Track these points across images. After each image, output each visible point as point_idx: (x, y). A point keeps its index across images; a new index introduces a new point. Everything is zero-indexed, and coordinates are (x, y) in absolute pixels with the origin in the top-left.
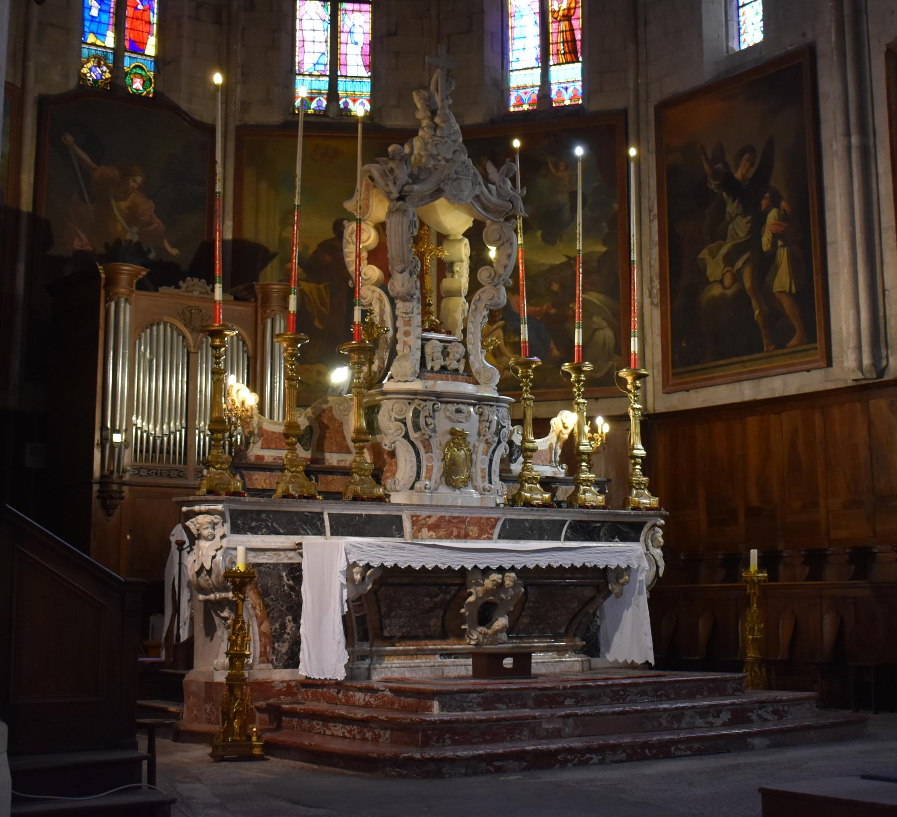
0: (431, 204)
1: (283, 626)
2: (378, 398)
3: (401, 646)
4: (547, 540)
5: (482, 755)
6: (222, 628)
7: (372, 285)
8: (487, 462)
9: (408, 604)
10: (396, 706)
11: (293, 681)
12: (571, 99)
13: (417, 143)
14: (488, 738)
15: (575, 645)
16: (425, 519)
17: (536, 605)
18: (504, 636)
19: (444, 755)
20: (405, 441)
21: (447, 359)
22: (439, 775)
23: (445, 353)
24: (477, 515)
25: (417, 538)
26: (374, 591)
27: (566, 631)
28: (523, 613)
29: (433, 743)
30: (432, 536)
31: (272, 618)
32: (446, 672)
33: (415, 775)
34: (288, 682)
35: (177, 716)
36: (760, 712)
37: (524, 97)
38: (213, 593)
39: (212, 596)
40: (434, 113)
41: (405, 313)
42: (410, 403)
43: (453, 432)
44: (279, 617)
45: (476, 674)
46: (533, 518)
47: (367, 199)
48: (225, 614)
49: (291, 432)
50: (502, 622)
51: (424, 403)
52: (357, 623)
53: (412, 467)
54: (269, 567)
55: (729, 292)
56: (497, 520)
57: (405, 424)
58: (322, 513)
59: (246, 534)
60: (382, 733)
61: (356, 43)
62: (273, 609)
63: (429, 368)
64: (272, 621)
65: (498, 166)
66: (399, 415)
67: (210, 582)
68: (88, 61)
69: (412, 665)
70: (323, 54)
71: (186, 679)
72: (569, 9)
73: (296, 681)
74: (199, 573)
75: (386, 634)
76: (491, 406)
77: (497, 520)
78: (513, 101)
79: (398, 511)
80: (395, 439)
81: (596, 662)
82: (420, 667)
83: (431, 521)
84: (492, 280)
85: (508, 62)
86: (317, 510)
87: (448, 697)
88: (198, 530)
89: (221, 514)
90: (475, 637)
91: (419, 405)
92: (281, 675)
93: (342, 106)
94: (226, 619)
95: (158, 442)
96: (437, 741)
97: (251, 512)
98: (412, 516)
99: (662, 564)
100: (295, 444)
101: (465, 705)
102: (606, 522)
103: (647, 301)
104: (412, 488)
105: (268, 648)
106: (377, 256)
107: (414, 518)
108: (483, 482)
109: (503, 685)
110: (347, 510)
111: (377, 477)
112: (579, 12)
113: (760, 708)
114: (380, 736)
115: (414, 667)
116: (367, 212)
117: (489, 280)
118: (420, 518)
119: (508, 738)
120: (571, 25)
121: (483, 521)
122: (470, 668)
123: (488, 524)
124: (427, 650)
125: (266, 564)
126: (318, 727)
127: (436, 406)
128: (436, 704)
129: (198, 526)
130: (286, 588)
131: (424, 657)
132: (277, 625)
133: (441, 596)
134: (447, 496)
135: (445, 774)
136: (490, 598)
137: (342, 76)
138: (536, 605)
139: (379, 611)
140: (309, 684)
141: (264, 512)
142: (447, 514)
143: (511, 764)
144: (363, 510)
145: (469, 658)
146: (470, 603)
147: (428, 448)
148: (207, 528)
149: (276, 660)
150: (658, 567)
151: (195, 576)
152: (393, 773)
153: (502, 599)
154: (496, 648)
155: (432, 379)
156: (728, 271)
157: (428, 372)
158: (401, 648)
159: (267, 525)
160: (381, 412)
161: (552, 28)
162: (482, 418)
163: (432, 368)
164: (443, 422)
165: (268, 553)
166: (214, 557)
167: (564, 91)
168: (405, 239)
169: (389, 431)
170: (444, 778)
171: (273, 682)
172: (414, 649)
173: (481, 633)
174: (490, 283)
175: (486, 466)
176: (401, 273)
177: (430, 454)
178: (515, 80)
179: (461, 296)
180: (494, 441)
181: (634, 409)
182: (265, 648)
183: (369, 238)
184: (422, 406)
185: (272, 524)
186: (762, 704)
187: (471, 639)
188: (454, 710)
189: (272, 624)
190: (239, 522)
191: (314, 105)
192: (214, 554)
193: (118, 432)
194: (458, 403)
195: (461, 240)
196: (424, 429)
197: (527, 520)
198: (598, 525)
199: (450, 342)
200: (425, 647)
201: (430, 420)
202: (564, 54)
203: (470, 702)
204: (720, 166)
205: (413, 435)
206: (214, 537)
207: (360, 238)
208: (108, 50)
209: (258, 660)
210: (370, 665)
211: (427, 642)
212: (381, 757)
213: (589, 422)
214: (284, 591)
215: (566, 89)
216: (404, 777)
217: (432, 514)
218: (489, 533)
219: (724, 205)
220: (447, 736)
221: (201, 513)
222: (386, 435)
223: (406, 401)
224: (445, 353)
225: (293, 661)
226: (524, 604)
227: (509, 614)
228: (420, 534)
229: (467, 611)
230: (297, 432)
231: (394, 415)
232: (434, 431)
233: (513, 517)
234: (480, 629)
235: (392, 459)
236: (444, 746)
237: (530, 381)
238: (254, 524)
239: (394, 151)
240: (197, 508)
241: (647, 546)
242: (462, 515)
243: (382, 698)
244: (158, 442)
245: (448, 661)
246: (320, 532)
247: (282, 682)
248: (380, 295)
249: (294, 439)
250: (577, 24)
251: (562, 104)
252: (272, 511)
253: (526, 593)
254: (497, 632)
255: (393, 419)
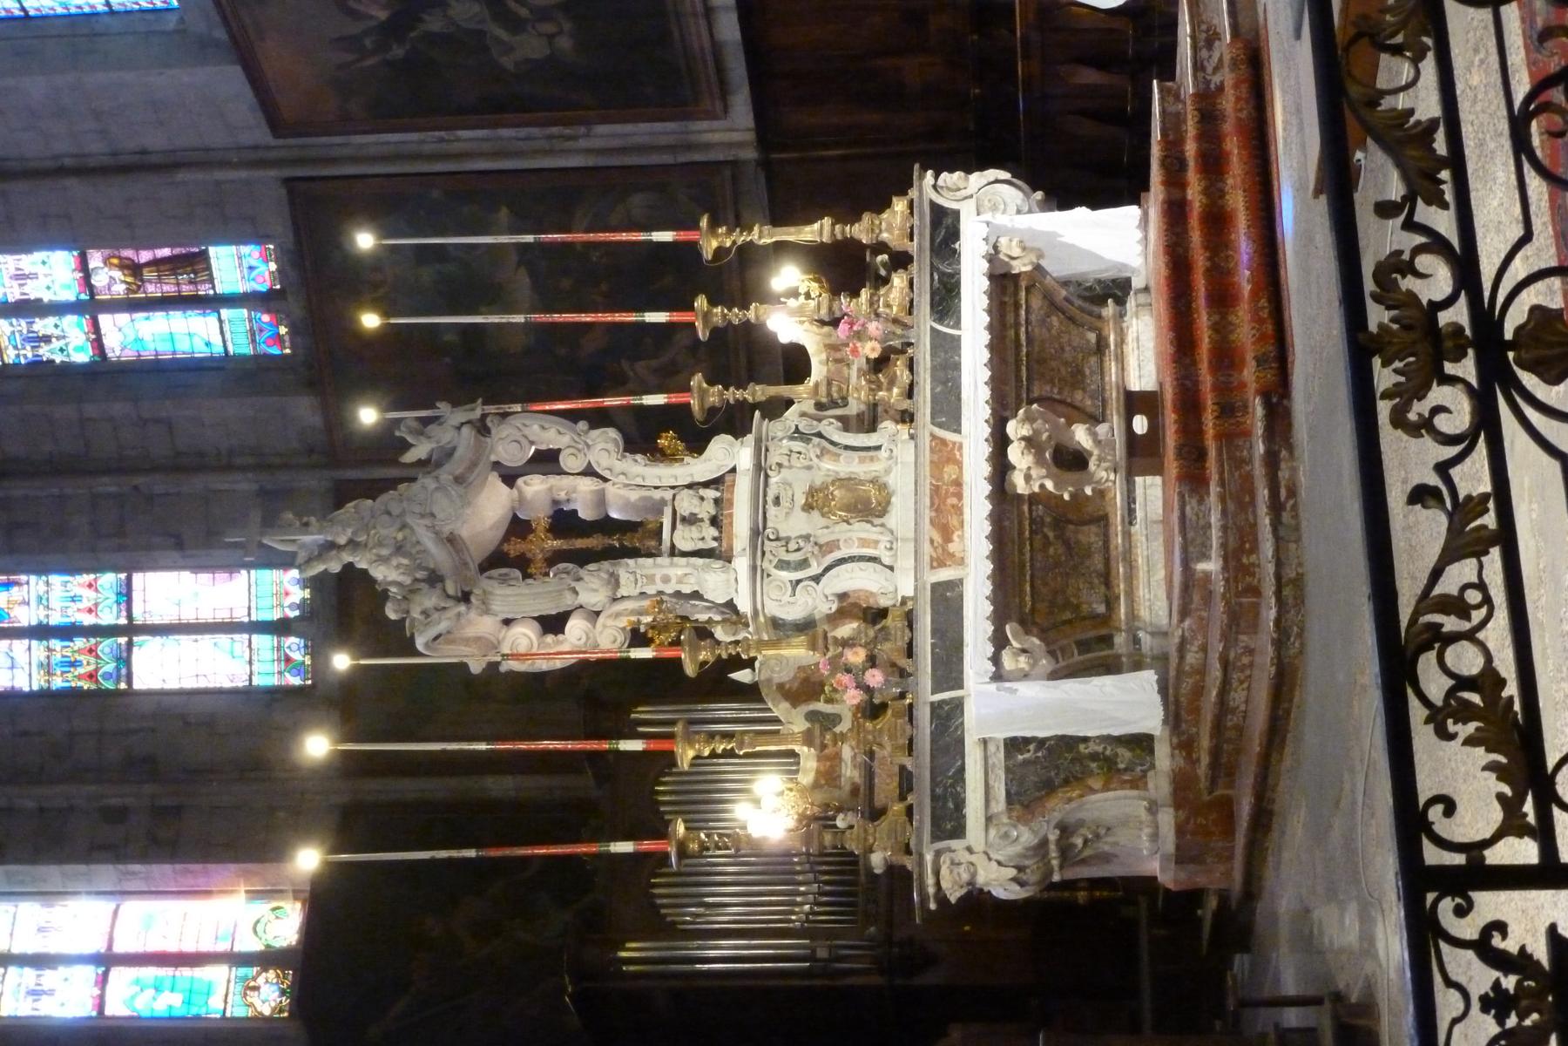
0: (468, 543)
1: (1094, 757)
2: (762, 619)
3: (1119, 586)
4: (960, 356)
5: (1271, 520)
6: (1100, 845)
7: (594, 627)
8: (850, 453)
9: (1059, 579)
10: (1205, 614)
11: (1171, 740)
12: (266, 261)
13: (379, 573)
14: (1247, 499)
15: (1114, 316)
16: (935, 549)
17: (1056, 381)
18: (1102, 429)
19: (1272, 575)
20: (824, 580)
21: (700, 516)
22: (1298, 582)
23: (691, 520)
24: (928, 469)
25: (962, 558)
26: (1043, 634)
27: (1091, 329)
28: (1069, 400)
29: (1256, 580)
30: (959, 536)
31: (1083, 773)
32: (1155, 518)
33: (1300, 617)
34: (1173, 748)
35: (1224, 897)
36: (1210, 70)
37: (266, 335)
38: (1049, 862)
39: (1055, 863)
40: (331, 546)
41: (636, 584)
42: (769, 575)
43: (808, 507)
44: (1082, 764)
45: (1157, 470)
46: (928, 381)
47: (467, 641)
48: (1079, 841)
49: (817, 741)
50: (1081, 435)
51: (768, 555)
52: (1088, 651)
53: (861, 569)
54: (1011, 781)
55: (567, 26)
56: (934, 437)
57: (799, 582)
58: (932, 704)
59: (964, 816)
60: (1242, 644)
61: (196, 594)
62: (1070, 772)
63: (715, 544)
64: (1088, 773)
65: (405, 446)
66: (786, 591)
67: (1035, 867)
68: (251, 1005)
69: (1146, 569)
70: (215, 644)
71: (1171, 886)
72: (122, 267)
73: (1171, 735)
74: (1022, 884)
75: (1101, 609)
76: (767, 450)
77: (934, 437)
78: (275, 351)
79: (924, 588)
80: (822, 596)
81: (1137, 283)
82: (1148, 557)
83: (938, 538)
84: (579, 450)
85: (212, 359)
86: (927, 710)
87: (1191, 549)
88: (962, 887)
89: (938, 854)
90: (1104, 474)
91: (770, 561)
92: (1164, 757)
93: (297, 613)
94: (1086, 842)
95: (828, 888)
96: (1253, 575)
97: (933, 809)
98: (932, 567)
99: (993, 174)
100: (835, 734)
101: (1202, 522)
102: (932, 264)
103: (582, 143)
104: (891, 568)
105: (1126, 778)
106: (553, 624)
107: (935, 564)
108: (878, 459)
109: (1171, 439)
110: (925, 658)
111: (877, 615)
112: (128, 253)
113: (1203, 69)
114: (1246, 647)
115: (1148, 565)
116: (486, 639)
117: (580, 456)
118: (934, 555)
119: (1248, 468)
120: (148, 264)
121: (936, 457)
122: (1149, 479)
123: (940, 451)
124: (1124, 546)
125: (1006, 784)
126: (1235, 719)
127: (771, 537)
128: (1202, 566)
129: (956, 887)
130: (1040, 754)
131: (1134, 550)
132: (1094, 765)
133: (1045, 530)
134: (901, 515)
135: (1298, 574)
136: (1047, 455)
137: (249, 615)
138: (1056, 381)
139: (1069, 622)
140: (1175, 716)
141: (933, 791)
142: (927, 514)
143: (1284, 474)
144: (925, 642)
145: (1134, 482)
146: (1056, 485)
147: (833, 546)
148: (959, 874)
149: (1142, 765)
150: (997, 181)
151: (1028, 888)
152: (1297, 645)
153: (1050, 437)
154: (1120, 442)
155: (730, 539)
156: (534, 27)
157: (720, 545)
158: (1122, 586)
159: (952, 785)
160: (783, 616)
161: (153, 290)
162: (786, 463)
163: (715, 539)
164: (791, 522)
165: (991, 782)
166: (999, 863)
167: (254, 273)
168: (527, 591)
169: (810, 604)
170: (1302, 575)
171: (1173, 770)
172: (1124, 567)
173: (1098, 466)
174: (585, 455)
175: (856, 455)
176: (576, 593)
177: (841, 543)
178: (241, 346)
179: (603, 490)
180: (819, 444)
181: (760, 237)
182: (1126, 782)
183: (525, 635)
184: (771, 557)
185: (950, 778)
186: (1198, 66)
187: (1107, 480)
188: (1209, 538)
189: (1091, 774)
190: (949, 827)
191: (297, 656)
192: (995, 863)
193: (814, 951)
194: (765, 502)
195: (520, 492)
196: (805, 554)
197: (932, 389)
198: (936, 277)
199: (674, 512)
200: (1120, 549)
201: (792, 546)
202: (196, 273)
203: (1197, 515)
204: (368, 42)
205: (815, 569)
206: (972, 864)
207: (526, 655)
208: (233, 977)
209: (1142, 793)
210: (1147, 632)
211: (1112, 547)
212: (1275, 661)
213: (782, 299)
214: (1044, 757)
215: (251, 268)
216: (1302, 630)
217: (927, 537)
218: (953, 449)
219: (432, 39)
220: (1245, 560)
221: (938, 884)
222: (816, 608)
223: (766, 580)
224: (691, 520)
225: (1141, 743)
226: (1055, 400)
227: (1070, 423)
228: (957, 554)
229: (1066, 490)
230: (817, 732)
231: (787, 598)
232: (807, 538)
233: (928, 411)
234: (1092, 466)
235: (849, 597)
236: (1259, 566)
237: (727, 390)
238: (951, 805)
239: (396, 611)
240: (931, 890)
241: (966, 198)
242: (928, 492)
243: (1193, 631)
244: (828, 888)
245: (1139, 514)
246: (958, 706)
247: (1173, 756)
248: (610, 616)
249: (828, 737)
250: (145, 256)
251: (276, 274)
252: (933, 779)
253: (1039, 400)
254: (1097, 442)
255: (792, 599)
